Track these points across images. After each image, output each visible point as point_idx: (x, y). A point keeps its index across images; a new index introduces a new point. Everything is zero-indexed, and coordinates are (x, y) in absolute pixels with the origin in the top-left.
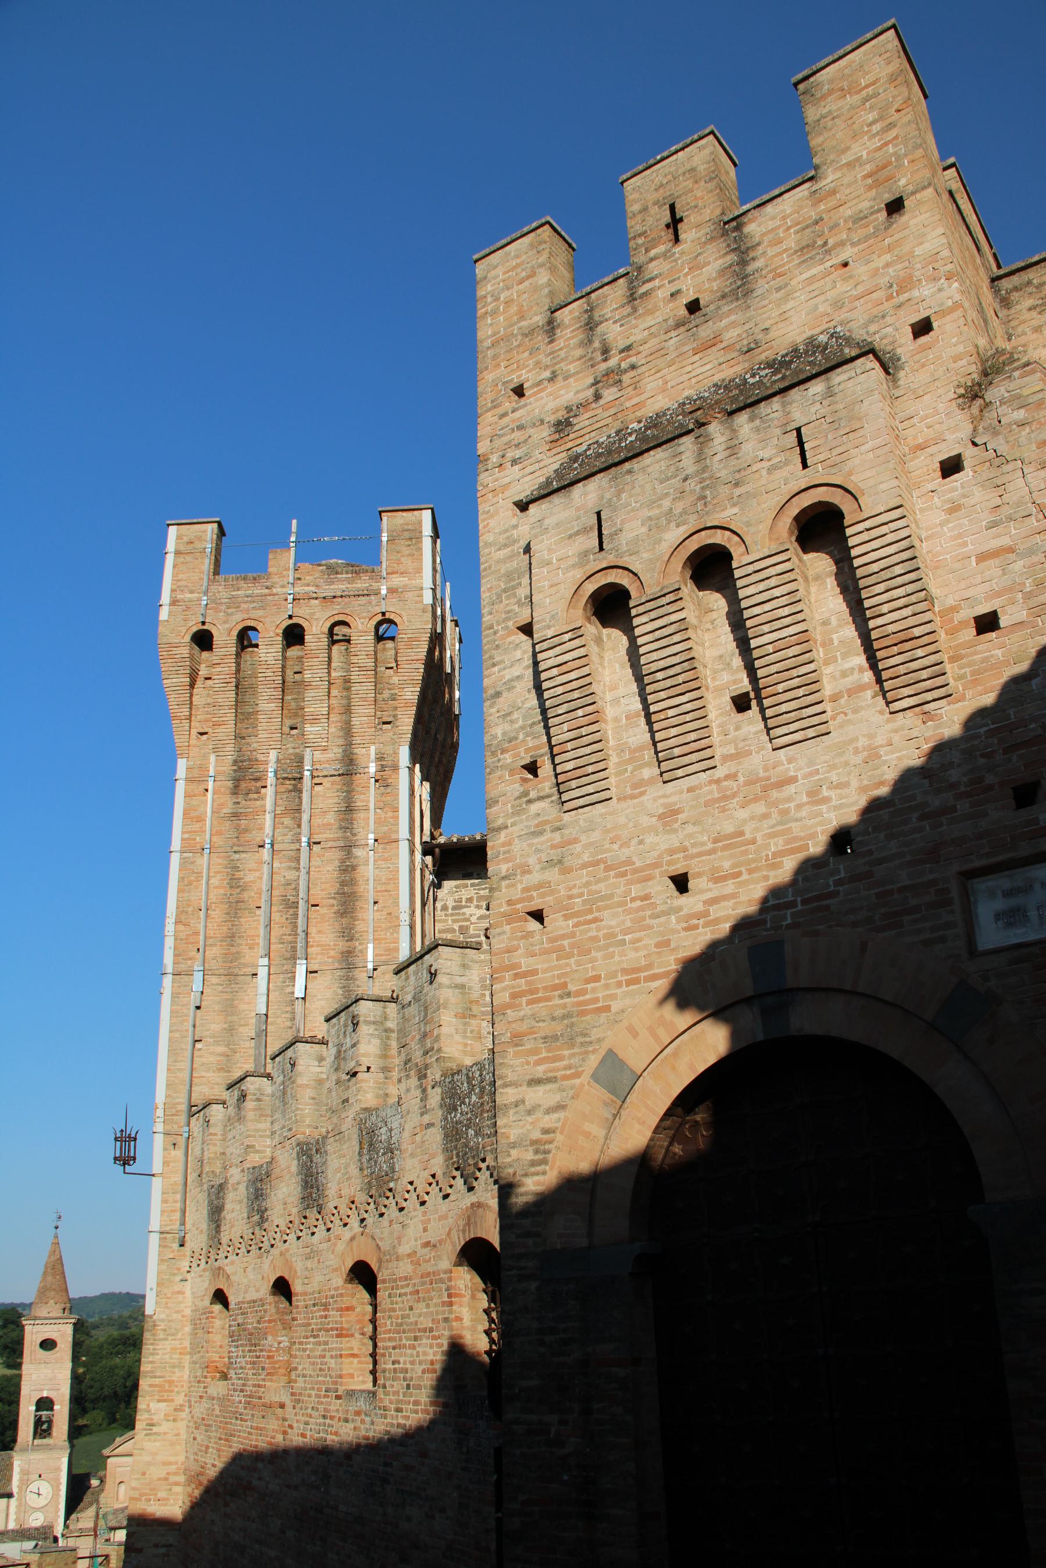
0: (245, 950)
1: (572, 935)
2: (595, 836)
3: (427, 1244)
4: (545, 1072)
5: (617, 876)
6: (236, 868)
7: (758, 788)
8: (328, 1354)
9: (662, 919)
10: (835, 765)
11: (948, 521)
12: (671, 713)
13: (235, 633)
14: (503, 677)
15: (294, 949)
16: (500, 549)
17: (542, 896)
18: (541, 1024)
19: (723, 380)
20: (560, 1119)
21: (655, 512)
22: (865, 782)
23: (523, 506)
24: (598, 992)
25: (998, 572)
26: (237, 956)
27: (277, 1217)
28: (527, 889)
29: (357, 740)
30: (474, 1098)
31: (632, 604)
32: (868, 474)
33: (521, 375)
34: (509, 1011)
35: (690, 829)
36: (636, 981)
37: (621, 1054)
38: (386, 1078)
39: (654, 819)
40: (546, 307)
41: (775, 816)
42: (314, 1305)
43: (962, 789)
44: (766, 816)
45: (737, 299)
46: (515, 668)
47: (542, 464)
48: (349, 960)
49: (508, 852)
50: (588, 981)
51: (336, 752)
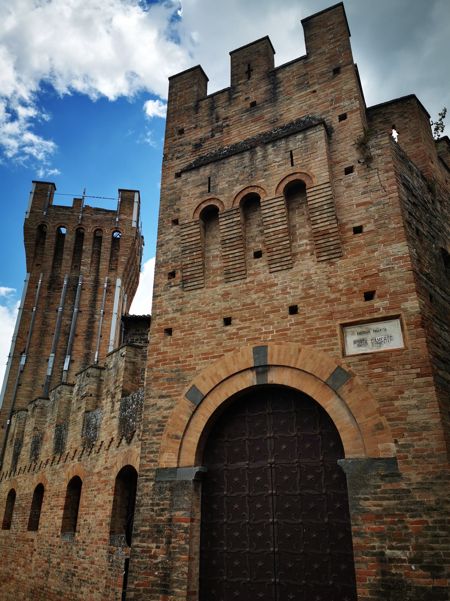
0: (45, 350)
1: (183, 339)
2: (196, 301)
3: (106, 468)
4: (166, 393)
5: (203, 317)
6: (46, 318)
7: (260, 287)
8: (56, 518)
9: (220, 335)
10: (293, 280)
11: (346, 191)
12: (230, 256)
13: (56, 228)
14: (165, 239)
15: (66, 351)
16: (168, 190)
17: (172, 323)
18: (166, 373)
19: (263, 133)
20: (170, 412)
21: (232, 179)
22: (305, 287)
23: (178, 175)
24: (191, 361)
25: (365, 211)
26: (42, 352)
27: (43, 458)
28: (166, 320)
29: (101, 274)
30: (134, 406)
31: (219, 213)
32: (317, 170)
33: (183, 125)
34: (154, 368)
35: (234, 301)
36: (207, 358)
37: (198, 387)
38: (97, 399)
39: (220, 296)
40: (196, 100)
41: (268, 298)
42: (53, 495)
43: (344, 292)
44: (264, 298)
45: (271, 102)
46: (170, 236)
47: (188, 160)
48: (88, 356)
49: (160, 305)
50: (187, 357)
51: (92, 278)
